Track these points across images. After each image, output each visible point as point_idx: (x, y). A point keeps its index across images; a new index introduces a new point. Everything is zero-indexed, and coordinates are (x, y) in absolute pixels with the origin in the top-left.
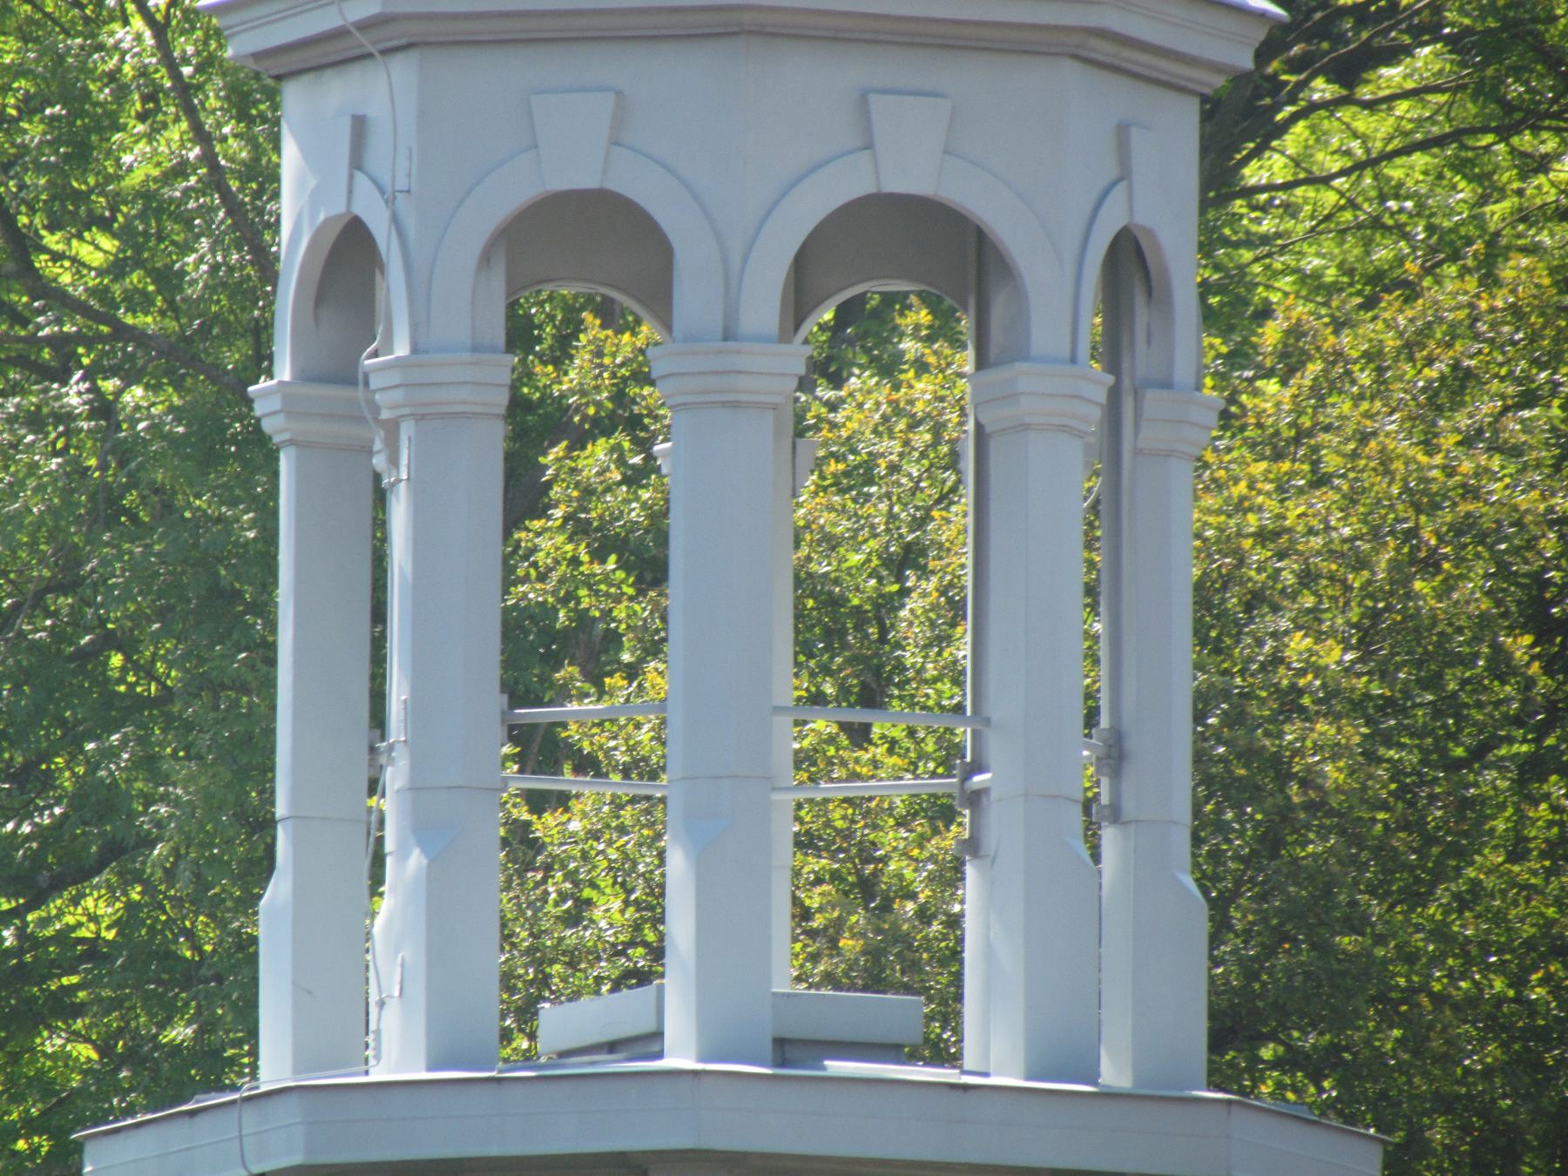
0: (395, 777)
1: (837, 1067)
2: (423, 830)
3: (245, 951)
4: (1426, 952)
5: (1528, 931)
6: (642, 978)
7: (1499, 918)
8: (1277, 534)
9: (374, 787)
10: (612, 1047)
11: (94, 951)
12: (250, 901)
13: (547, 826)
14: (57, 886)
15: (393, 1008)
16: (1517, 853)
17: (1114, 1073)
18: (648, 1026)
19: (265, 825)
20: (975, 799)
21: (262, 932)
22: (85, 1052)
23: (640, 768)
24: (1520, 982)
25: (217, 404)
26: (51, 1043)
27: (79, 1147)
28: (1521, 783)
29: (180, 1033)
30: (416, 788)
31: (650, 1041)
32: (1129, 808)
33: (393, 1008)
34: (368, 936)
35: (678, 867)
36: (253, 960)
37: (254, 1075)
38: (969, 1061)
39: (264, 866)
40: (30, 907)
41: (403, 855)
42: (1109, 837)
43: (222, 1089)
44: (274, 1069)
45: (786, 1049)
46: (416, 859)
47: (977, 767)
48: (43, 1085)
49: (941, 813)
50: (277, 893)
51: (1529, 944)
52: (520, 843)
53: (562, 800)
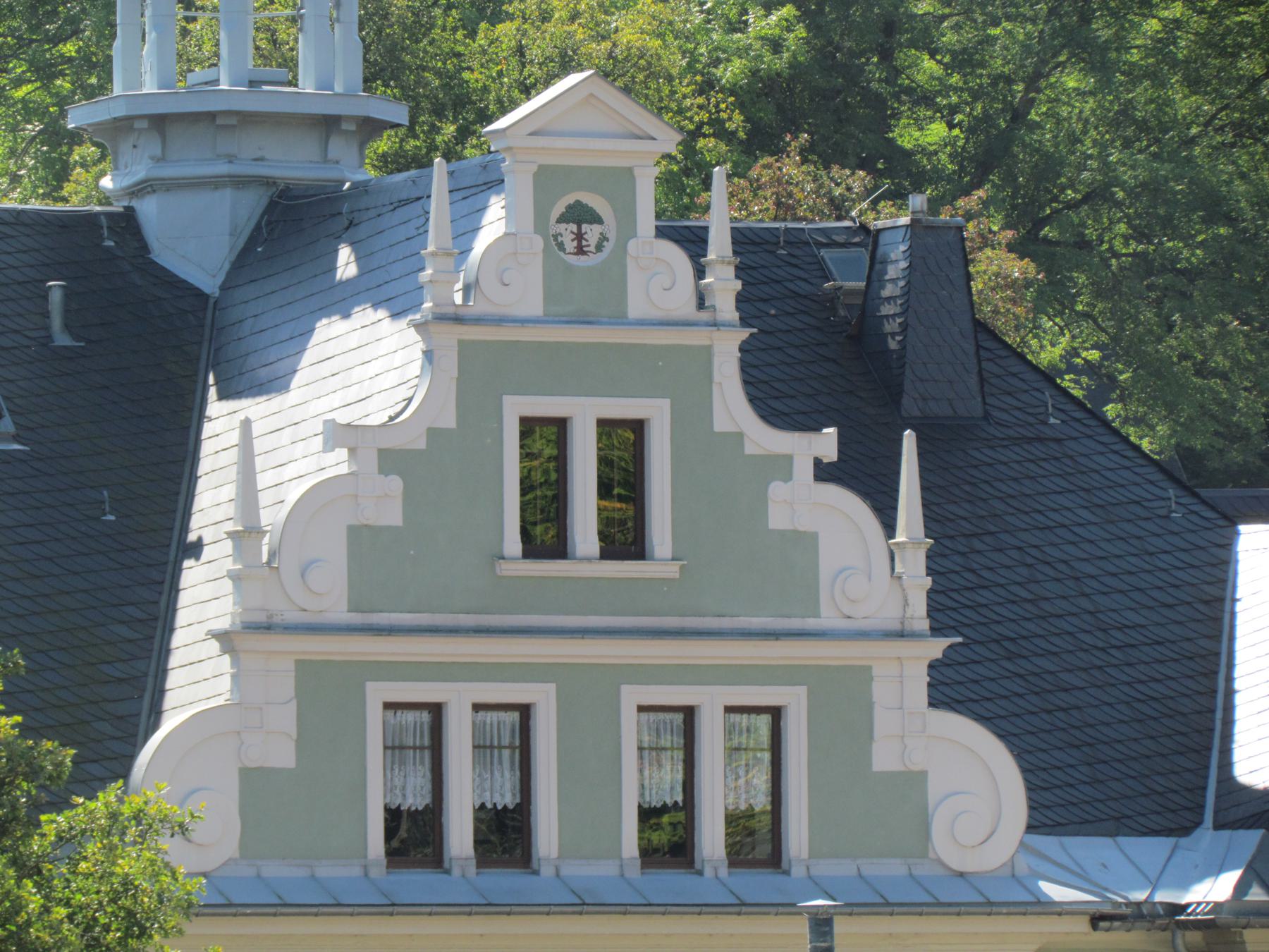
0: (148, 13)
1: (266, 88)
2: (155, 27)
3: (109, 59)
4: (1043, 134)
5: (447, 50)
6: (215, 65)
7: (439, 47)
8: (658, 730)
9: (142, 15)
10: (206, 83)
11: (70, 59)
12: (110, 46)
13: (190, 27)
14: (59, 42)
15: (148, 75)
16: (444, 29)
17: (338, 89)
18: (215, 77)
19: (113, 25)
20: (301, 16)
21: (113, 53)
22: (68, 85)
23: (215, 9)
24: (444, 63)
25: (751, 201)
26: (58, 82)
27: (66, 111)
28: (445, 11)
29: (93, 80)
30: (154, 16)
31: (216, 82)
32: (342, 18)
33: (148, 75)
34: (141, 56)
35: (223, 36)
36: (111, 61)
37: (112, 91)
38: (300, 86)
39: (113, 36)
40: (54, 47)
41: (150, 33)
42: (336, 26)
43: (104, 95)
44: (117, 89)
45: (252, 83)
46: (154, 34)
47: (302, 8)
48: (57, 95)
49: (294, 20)
50: (117, 43)
51: (448, 54)
52: (185, 33)
53: (194, 19)
